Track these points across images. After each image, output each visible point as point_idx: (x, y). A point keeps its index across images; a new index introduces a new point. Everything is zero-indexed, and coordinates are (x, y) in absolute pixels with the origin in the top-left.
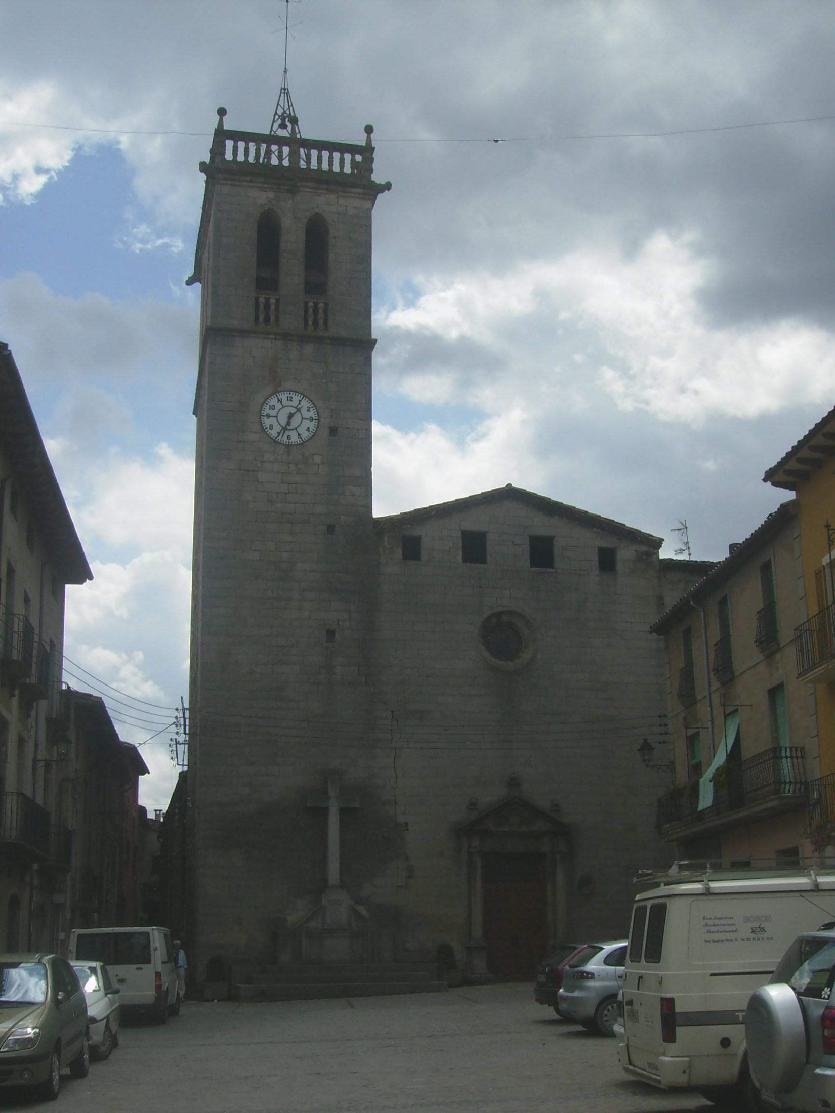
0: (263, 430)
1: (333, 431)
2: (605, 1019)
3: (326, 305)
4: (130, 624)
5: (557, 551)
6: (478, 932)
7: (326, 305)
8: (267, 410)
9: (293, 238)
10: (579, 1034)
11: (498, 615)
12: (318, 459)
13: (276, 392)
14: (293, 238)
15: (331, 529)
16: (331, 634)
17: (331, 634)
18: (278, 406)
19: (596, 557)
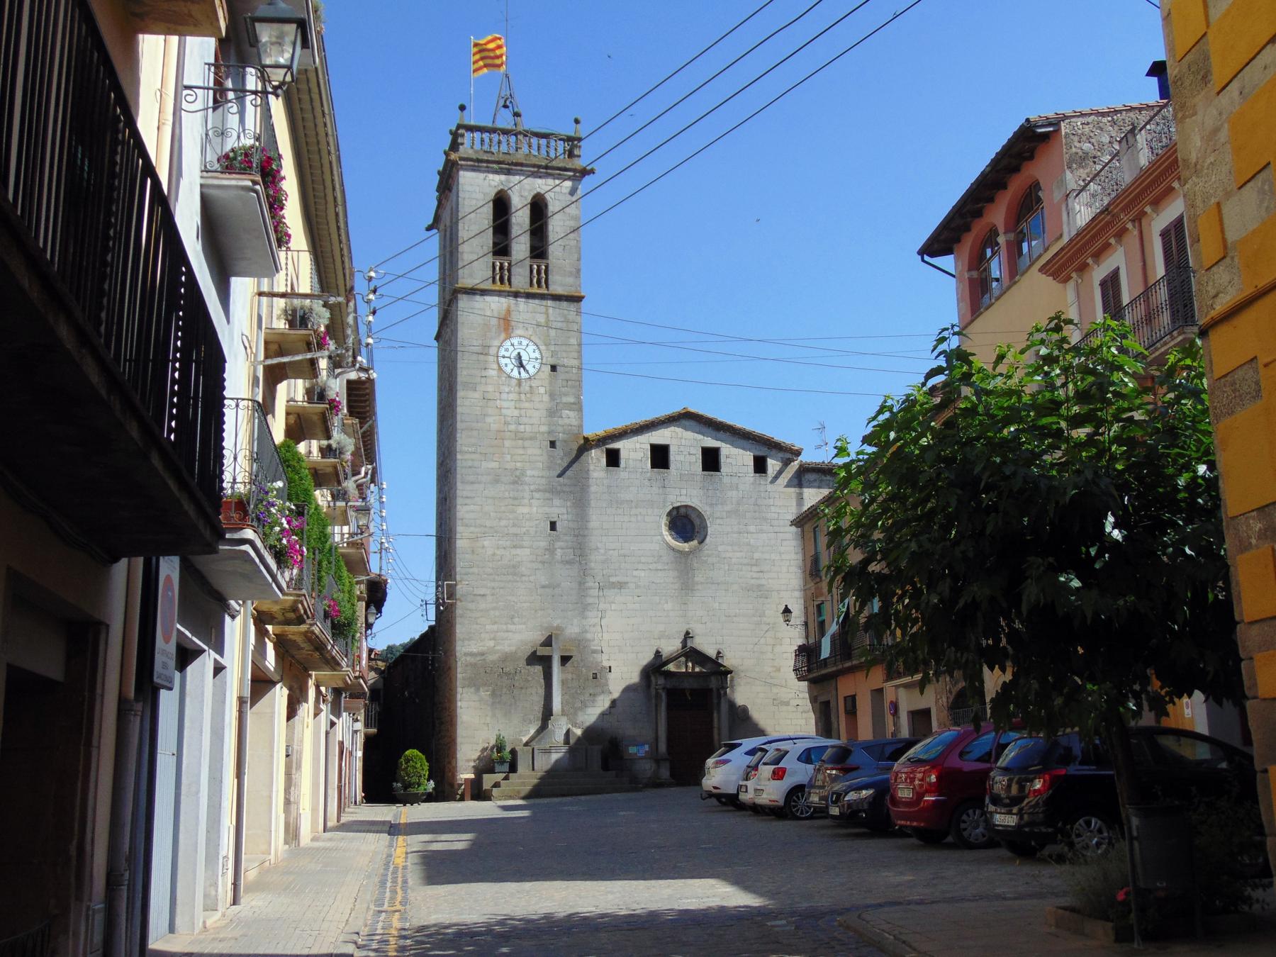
0: (500, 368)
1: (554, 368)
2: (963, 826)
3: (547, 267)
4: (525, 813)
5: (723, 459)
6: (663, 747)
7: (547, 267)
8: (502, 352)
9: (520, 219)
10: (858, 836)
11: (678, 508)
12: (542, 390)
13: (509, 337)
14: (520, 219)
15: (553, 444)
16: (553, 526)
17: (553, 526)
18: (511, 349)
19: (752, 463)
